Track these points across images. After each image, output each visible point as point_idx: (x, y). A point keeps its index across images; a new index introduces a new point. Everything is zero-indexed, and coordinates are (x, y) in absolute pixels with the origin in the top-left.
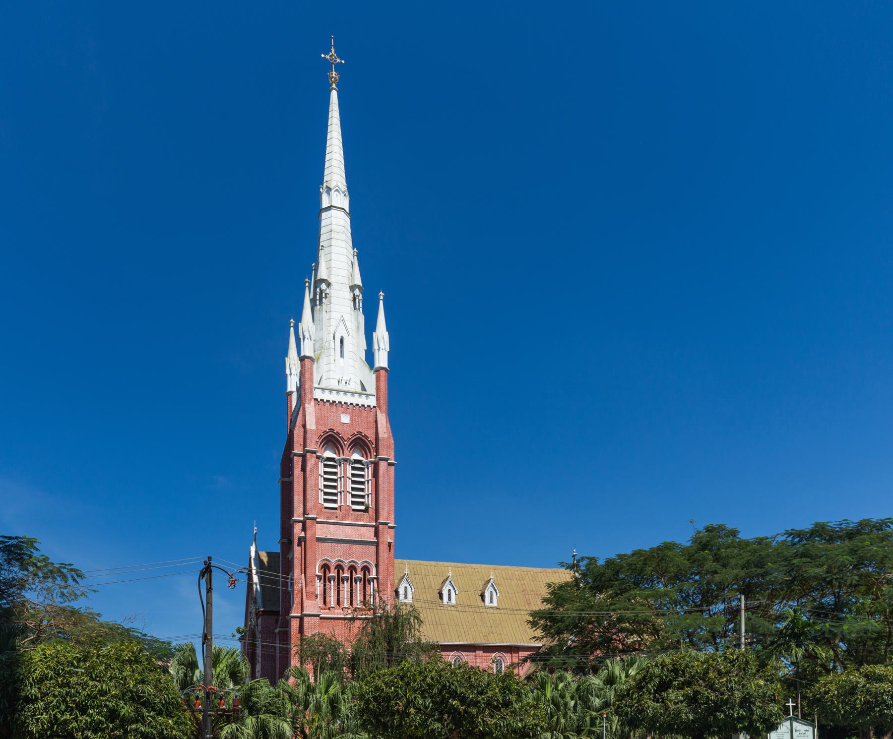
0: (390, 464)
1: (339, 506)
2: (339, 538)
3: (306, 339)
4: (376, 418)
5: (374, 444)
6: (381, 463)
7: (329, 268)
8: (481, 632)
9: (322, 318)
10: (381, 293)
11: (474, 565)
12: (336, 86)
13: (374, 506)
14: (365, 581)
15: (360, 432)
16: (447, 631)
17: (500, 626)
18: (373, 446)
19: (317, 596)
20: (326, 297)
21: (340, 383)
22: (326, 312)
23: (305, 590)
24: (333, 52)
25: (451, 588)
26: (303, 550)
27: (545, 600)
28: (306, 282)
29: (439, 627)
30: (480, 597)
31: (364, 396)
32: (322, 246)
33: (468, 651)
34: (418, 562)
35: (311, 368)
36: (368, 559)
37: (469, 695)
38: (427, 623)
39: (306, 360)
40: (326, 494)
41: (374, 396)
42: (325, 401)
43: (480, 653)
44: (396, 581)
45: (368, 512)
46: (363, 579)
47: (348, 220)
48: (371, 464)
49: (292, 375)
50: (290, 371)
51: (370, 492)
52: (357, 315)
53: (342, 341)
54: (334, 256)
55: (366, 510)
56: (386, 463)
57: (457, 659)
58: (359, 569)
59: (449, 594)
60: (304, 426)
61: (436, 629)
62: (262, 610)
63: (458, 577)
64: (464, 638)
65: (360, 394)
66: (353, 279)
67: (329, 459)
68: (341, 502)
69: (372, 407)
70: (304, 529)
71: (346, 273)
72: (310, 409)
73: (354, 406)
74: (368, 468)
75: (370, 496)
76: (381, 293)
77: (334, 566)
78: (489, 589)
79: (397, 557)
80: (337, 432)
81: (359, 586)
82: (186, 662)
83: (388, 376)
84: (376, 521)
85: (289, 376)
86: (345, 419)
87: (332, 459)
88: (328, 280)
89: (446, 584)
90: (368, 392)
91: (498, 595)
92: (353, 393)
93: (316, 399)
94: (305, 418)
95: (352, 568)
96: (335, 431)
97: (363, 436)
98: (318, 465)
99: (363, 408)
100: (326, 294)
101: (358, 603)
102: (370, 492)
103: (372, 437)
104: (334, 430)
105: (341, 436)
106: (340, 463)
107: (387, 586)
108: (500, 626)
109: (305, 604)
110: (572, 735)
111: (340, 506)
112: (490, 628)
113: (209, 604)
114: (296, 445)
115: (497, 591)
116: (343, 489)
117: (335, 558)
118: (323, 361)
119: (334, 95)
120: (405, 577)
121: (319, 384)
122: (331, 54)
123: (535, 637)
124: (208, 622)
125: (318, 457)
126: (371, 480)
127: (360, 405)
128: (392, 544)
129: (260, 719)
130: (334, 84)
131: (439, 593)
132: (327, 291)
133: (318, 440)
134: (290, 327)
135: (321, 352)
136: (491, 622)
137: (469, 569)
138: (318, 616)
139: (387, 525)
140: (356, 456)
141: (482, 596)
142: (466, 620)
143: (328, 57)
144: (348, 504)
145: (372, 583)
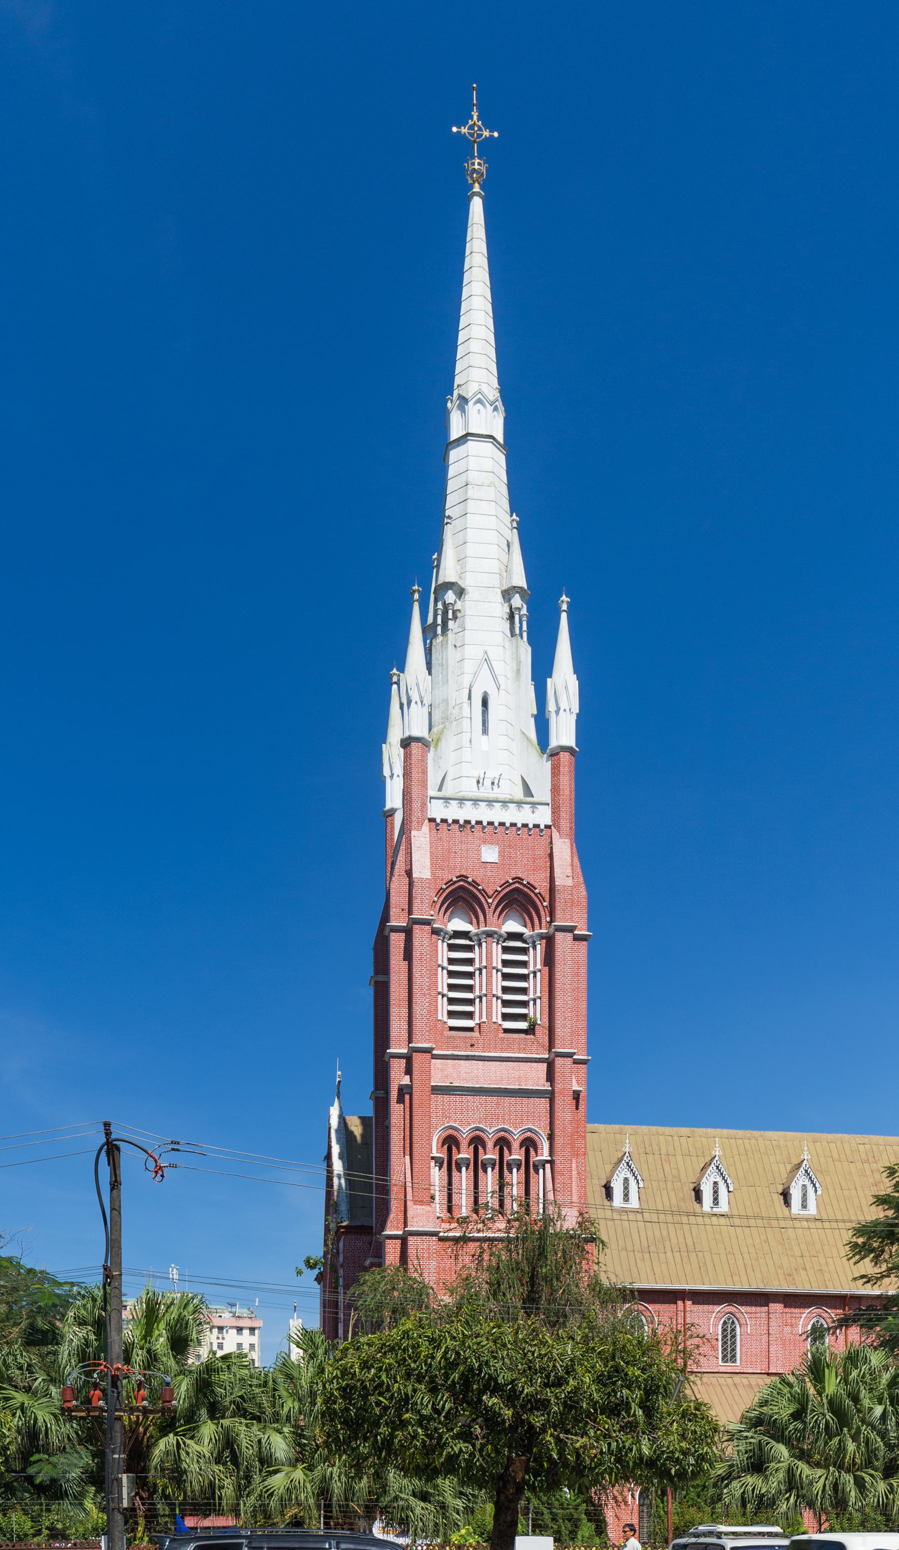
0: (577, 938)
1: (477, 1024)
2: (477, 1086)
3: (413, 703)
4: (552, 848)
5: (547, 899)
6: (559, 936)
7: (461, 560)
8: (781, 1267)
9: (447, 659)
10: (564, 598)
11: (770, 1134)
12: (481, 189)
13: (546, 1020)
14: (529, 1168)
15: (519, 878)
16: (709, 1265)
17: (821, 1256)
18: (545, 904)
19: (433, 1198)
20: (455, 618)
21: (480, 785)
22: (455, 646)
23: (551, 1185)
24: (475, 118)
25: (719, 1179)
26: (408, 1109)
27: (882, 1201)
28: (414, 591)
29: (693, 1258)
30: (782, 1197)
31: (527, 807)
32: (449, 517)
33: (751, 1305)
34: (654, 1129)
35: (424, 760)
36: (534, 1124)
37: (523, 1387)
38: (614, 1246)
39: (413, 744)
40: (451, 1001)
41: (548, 804)
42: (450, 821)
43: (776, 1307)
44: (609, 1167)
45: (534, 1034)
46: (523, 1163)
47: (502, 459)
48: (540, 940)
49: (395, 776)
50: (391, 771)
51: (538, 994)
52: (517, 648)
53: (485, 703)
54: (471, 535)
55: (531, 1031)
56: (569, 936)
57: (729, 1319)
58: (515, 1145)
59: (716, 1192)
60: (409, 873)
61: (685, 1260)
62: (344, 1224)
63: (737, 1157)
64: (744, 1278)
65: (519, 803)
66: (510, 577)
67: (457, 934)
68: (481, 1017)
69: (542, 827)
70: (409, 1071)
71: (495, 566)
72: (421, 838)
73: (507, 829)
74: (534, 948)
75: (538, 1001)
76: (564, 598)
77: (468, 1140)
78: (622, 1173)
79: (591, 1119)
80: (473, 881)
81: (515, 1177)
82: (90, 1319)
83: (577, 762)
84: (550, 1050)
85: (388, 780)
86: (490, 854)
87: (465, 935)
88: (460, 583)
89: (708, 1172)
90: (535, 799)
91: (819, 1192)
92: (505, 803)
93: (432, 820)
94: (411, 858)
95: (503, 1143)
96: (470, 880)
97: (524, 885)
98: (437, 947)
99: (526, 829)
100: (454, 612)
101: (464, 1208)
102: (538, 994)
103: (542, 887)
104: (467, 878)
105: (480, 887)
106: (480, 940)
107: (571, 1178)
108: (821, 1256)
109: (410, 1213)
110: (872, 1475)
111: (479, 1025)
112: (799, 1259)
113: (115, 1212)
114: (393, 911)
115: (817, 1185)
116: (484, 992)
117: (469, 1124)
118: (448, 744)
119: (477, 207)
120: (625, 1158)
121: (440, 789)
122: (470, 122)
123: (862, 1277)
124: (113, 1246)
125: (436, 932)
126: (540, 971)
127: (519, 825)
128: (582, 1095)
129: (222, 1427)
130: (477, 185)
131: (694, 1189)
132: (458, 606)
133: (436, 899)
134: (392, 684)
135: (445, 727)
136: (803, 1246)
137: (761, 1141)
138: (435, 1234)
139: (571, 1057)
140: (512, 926)
141: (786, 1195)
142: (750, 1241)
143: (464, 130)
144: (494, 1020)
145: (541, 1171)
